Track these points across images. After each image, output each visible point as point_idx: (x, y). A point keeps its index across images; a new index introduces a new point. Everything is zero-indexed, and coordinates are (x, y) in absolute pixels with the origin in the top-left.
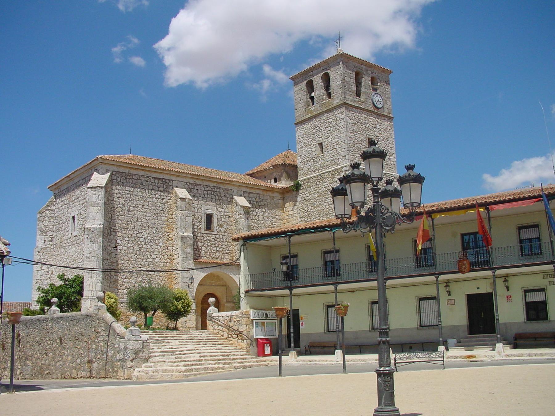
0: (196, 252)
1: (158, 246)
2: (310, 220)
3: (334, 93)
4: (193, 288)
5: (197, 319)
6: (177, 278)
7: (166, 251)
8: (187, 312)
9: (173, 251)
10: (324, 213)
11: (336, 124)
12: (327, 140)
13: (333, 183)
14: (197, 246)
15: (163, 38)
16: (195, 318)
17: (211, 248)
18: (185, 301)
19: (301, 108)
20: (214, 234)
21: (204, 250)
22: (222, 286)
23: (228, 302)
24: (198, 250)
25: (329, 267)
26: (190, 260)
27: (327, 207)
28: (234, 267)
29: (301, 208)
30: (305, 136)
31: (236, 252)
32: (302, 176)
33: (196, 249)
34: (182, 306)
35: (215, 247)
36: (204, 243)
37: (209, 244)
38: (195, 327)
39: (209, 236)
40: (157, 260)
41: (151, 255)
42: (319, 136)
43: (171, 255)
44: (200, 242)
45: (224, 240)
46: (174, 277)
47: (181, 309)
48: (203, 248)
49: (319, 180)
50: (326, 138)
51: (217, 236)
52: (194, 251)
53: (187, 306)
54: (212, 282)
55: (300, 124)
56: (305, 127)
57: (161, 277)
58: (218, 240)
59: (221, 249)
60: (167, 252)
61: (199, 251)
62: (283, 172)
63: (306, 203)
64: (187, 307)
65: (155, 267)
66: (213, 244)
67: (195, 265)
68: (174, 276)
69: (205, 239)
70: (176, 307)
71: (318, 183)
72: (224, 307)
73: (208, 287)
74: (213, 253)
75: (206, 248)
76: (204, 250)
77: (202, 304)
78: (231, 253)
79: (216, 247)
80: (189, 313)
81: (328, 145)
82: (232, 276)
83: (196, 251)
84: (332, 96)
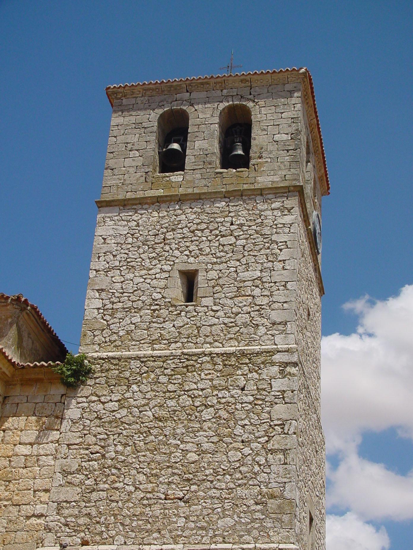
2: (107, 486)
3: (260, 157)
10: (174, 474)
11: (257, 232)
12: (217, 267)
13: (227, 389)
15: (341, 334)
19: (132, 170)
27: (192, 456)
29: (78, 441)
30: (130, 240)
32: (97, 348)
42: (187, 253)
49: (168, 371)
50: (215, 263)
55: (117, 209)
56: (134, 218)
62: (11, 324)
63: (99, 430)
71: (163, 379)
81: (221, 282)
84: (252, 162)
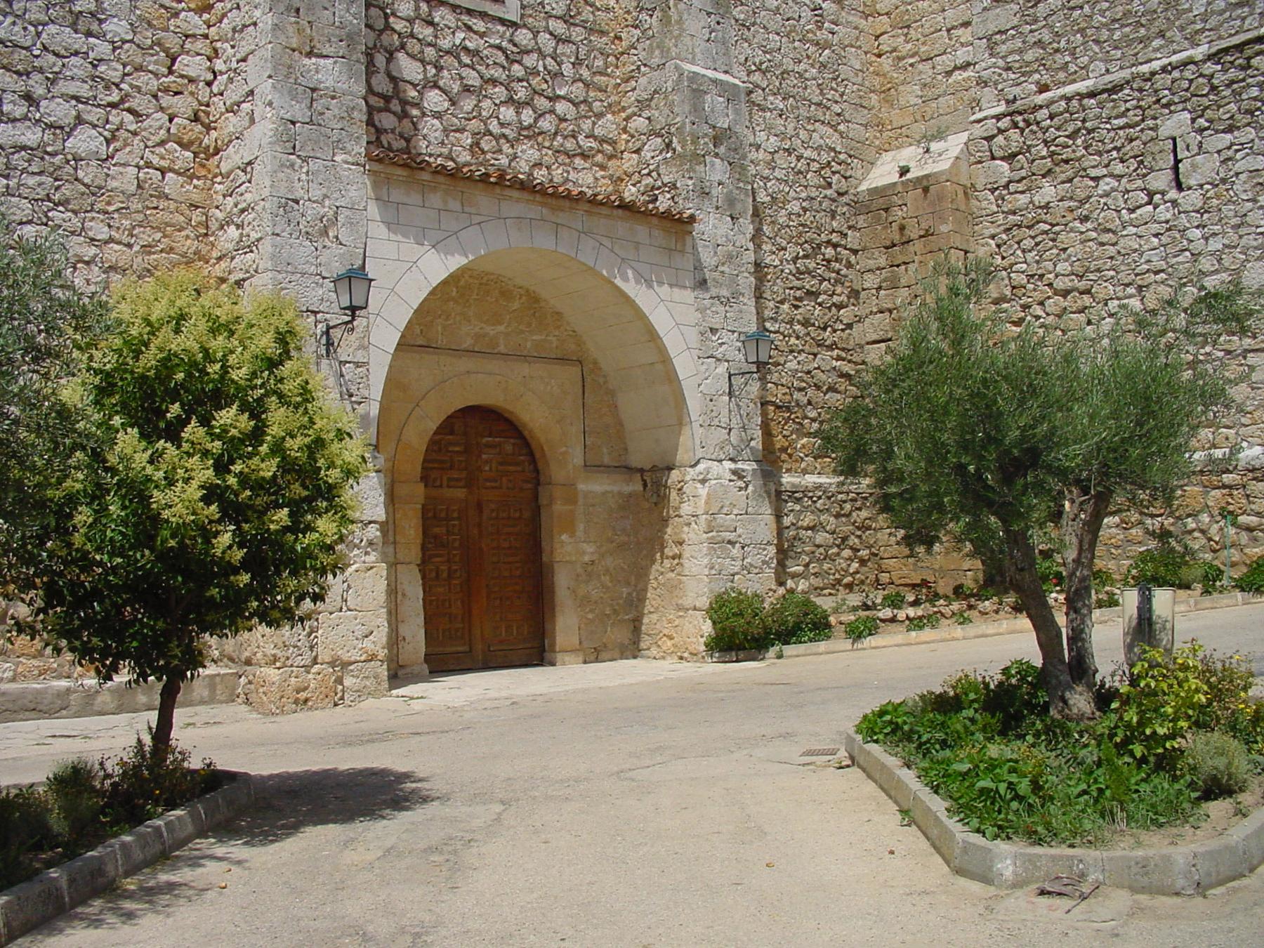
0: (387, 121)
1: (89, 34)
4: (360, 356)
5: (393, 591)
6: (239, 283)
7: (155, 84)
8: (297, 564)
9: (215, 89)
14: (394, 80)
16: (382, 585)
17: (486, 104)
18: (257, 435)
20: (502, 21)
21: (438, 115)
22: (562, 360)
23: (592, 467)
24: (395, 106)
25: (452, 483)
26: (338, 145)
28: (641, 231)
31: (638, 151)
33: (387, 99)
34: (211, 494)
35: (510, 101)
36: (439, 69)
37: (473, 79)
38: (382, 653)
39: (469, 28)
40: (85, 141)
41: (28, 98)
43: (196, 119)
44: (412, 57)
45: (567, 69)
46: (223, 280)
47: (208, 535)
48: (434, 99)
51: (523, 37)
52: (371, 110)
53: (298, 490)
54: (491, 330)
57: (115, 277)
58: (530, 60)
59: (546, 124)
60: (166, 90)
61: (404, 115)
64: (298, 509)
65: (67, 191)
66: (494, 82)
67: (376, 185)
68: (219, 270)
69: (445, 43)
70: (136, 491)
72: (572, 500)
73: (464, 364)
74: (497, 138)
75: (453, 103)
76: (438, 115)
77: (425, 479)
78: (610, 157)
79: (519, 106)
80: (307, 582)
82: (630, 287)
83: (388, 110)
